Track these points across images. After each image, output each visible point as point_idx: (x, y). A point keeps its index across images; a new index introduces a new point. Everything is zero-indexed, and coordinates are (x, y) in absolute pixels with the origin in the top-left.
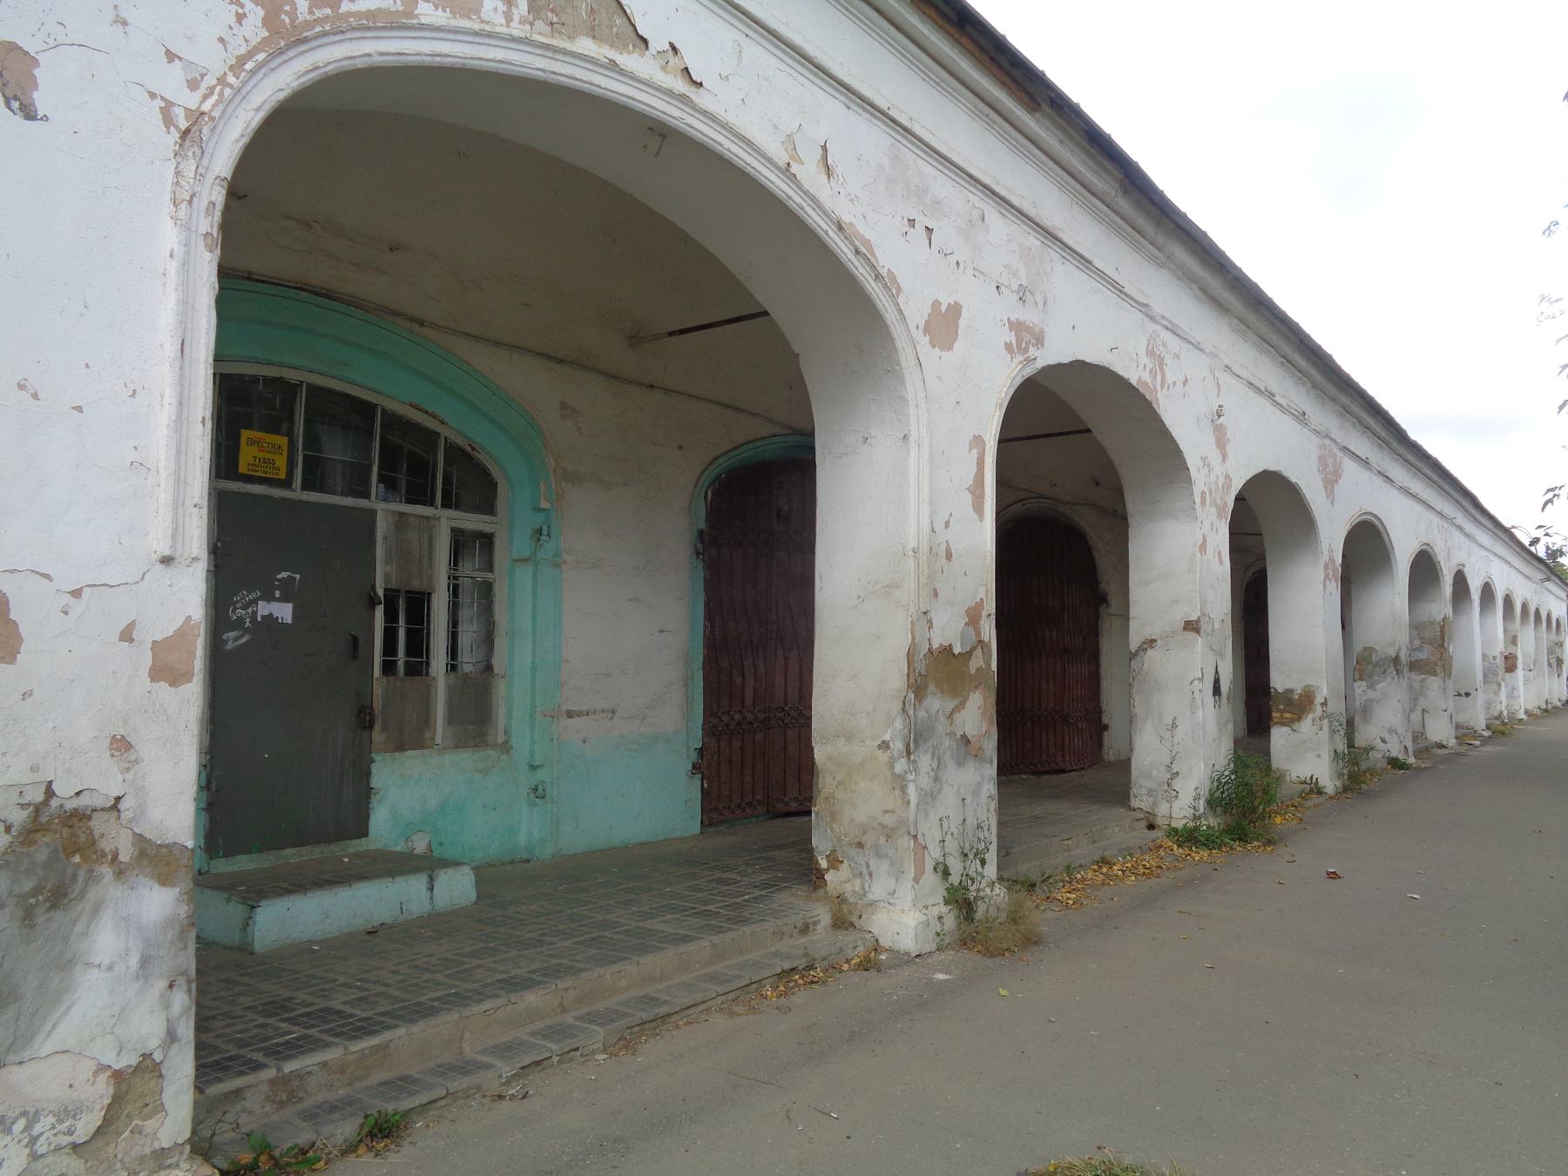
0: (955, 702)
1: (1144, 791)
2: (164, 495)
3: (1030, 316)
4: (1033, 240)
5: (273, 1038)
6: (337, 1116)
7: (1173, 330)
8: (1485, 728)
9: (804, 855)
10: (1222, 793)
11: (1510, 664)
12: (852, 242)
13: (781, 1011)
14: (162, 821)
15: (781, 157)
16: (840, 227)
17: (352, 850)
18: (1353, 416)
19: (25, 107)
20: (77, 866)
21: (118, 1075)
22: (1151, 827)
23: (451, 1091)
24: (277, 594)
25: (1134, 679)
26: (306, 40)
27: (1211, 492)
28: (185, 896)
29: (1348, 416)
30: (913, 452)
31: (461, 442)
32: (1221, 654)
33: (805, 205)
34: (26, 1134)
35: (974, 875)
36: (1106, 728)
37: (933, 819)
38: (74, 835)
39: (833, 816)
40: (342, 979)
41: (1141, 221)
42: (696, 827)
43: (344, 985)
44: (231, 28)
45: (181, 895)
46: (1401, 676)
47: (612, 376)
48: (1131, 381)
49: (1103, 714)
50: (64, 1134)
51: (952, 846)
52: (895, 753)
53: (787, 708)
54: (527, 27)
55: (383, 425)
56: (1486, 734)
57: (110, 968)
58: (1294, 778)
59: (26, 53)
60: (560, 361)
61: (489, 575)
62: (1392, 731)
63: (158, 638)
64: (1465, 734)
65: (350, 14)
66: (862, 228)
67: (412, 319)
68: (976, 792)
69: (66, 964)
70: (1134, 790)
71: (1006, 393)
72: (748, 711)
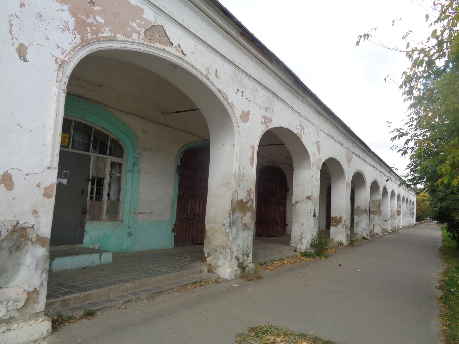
0: (243, 215)
1: (294, 242)
2: (49, 152)
3: (268, 115)
4: (270, 95)
5: (61, 291)
6: (78, 310)
7: (307, 119)
8: (390, 230)
9: (201, 254)
10: (315, 243)
11: (399, 213)
12: (222, 95)
13: (193, 292)
14: (43, 231)
15: (205, 73)
16: (219, 91)
17: (78, 247)
18: (356, 144)
19: (24, 58)
20: (23, 241)
21: (29, 293)
22: (295, 251)
23: (107, 306)
24: (63, 176)
25: (293, 211)
26: (90, 43)
27: (315, 163)
28: (47, 250)
29: (355, 144)
30: (236, 149)
31: (115, 138)
32: (316, 206)
33: (210, 85)
34: (6, 305)
35: (245, 260)
36: (287, 225)
37: (236, 245)
38: (22, 233)
39: (210, 243)
40: (77, 279)
41: (299, 91)
42: (172, 246)
43: (78, 280)
44: (72, 40)
45: (46, 250)
46: (367, 215)
47: (157, 123)
48: (295, 133)
49: (286, 221)
50: (15, 306)
51: (240, 252)
52: (227, 227)
53: (199, 215)
54: (143, 40)
55: (94, 132)
56: (391, 232)
57: (29, 266)
58: (336, 241)
59: (25, 46)
60: (143, 118)
61: (120, 174)
62: (364, 229)
63: (46, 187)
64: (384, 231)
65: (101, 37)
66: (225, 91)
67: (104, 105)
68: (247, 238)
69: (18, 265)
70: (292, 241)
71: (261, 135)
72: (188, 215)
